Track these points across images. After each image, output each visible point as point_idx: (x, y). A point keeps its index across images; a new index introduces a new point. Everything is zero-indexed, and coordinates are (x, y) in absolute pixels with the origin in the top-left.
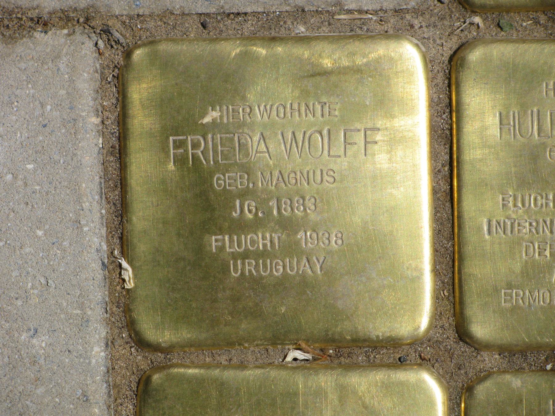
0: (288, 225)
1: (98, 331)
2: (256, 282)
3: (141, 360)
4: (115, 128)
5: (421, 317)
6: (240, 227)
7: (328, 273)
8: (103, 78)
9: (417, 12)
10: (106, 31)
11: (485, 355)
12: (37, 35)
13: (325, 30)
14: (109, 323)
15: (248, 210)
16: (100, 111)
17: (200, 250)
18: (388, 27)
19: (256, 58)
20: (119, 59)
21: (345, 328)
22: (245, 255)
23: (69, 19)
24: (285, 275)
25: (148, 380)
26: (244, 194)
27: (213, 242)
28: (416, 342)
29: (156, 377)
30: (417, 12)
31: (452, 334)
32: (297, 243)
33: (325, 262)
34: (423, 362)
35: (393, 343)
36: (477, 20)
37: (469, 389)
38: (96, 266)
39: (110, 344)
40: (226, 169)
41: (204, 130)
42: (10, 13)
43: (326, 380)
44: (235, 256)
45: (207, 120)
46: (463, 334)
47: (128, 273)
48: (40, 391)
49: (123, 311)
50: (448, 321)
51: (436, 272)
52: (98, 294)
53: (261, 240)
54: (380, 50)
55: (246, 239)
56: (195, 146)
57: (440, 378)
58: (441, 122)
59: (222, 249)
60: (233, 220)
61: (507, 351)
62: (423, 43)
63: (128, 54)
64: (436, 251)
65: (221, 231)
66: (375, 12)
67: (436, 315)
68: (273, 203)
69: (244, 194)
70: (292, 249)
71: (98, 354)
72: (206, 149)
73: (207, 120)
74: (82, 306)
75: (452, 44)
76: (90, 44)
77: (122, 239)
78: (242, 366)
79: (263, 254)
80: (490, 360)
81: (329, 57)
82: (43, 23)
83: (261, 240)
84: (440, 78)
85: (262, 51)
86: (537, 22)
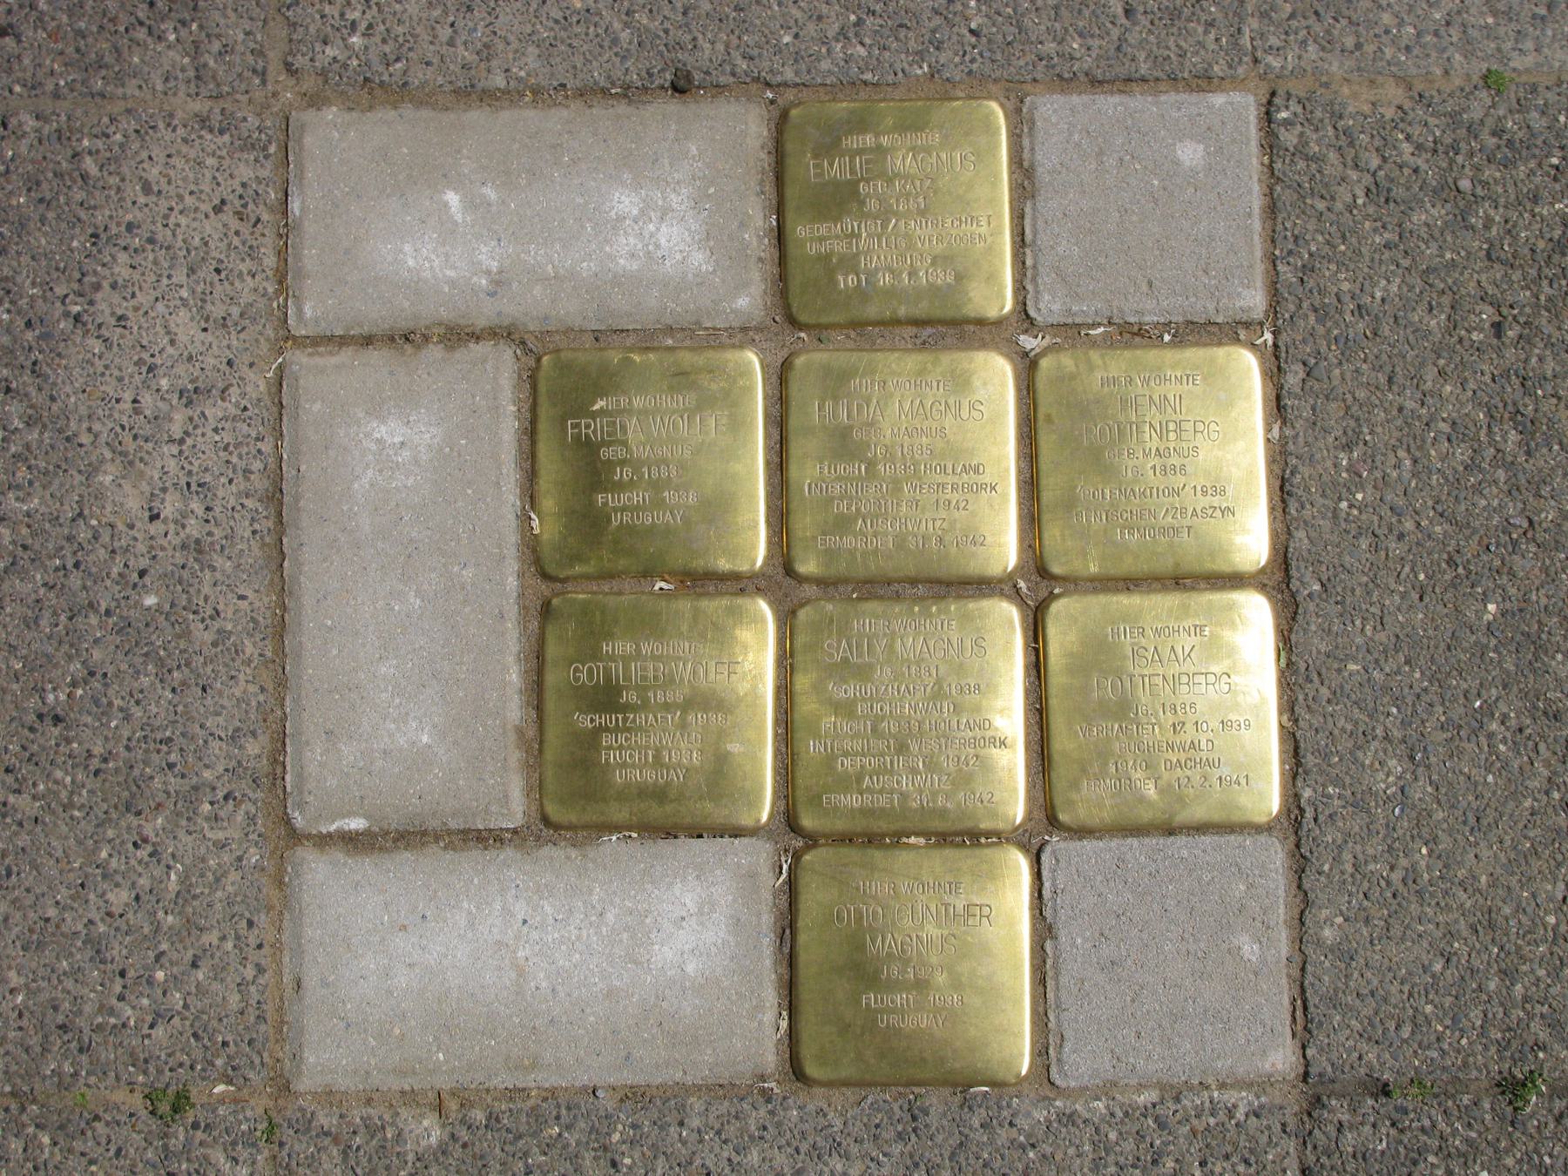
0: (657, 486)
1: (512, 566)
2: (630, 530)
3: (544, 588)
4: (528, 415)
5: (1018, 811)
6: (620, 487)
7: (687, 521)
8: (520, 376)
9: (758, 329)
10: (523, 343)
11: (806, 586)
12: (471, 345)
13: (688, 343)
14: (521, 560)
15: (625, 474)
16: (517, 401)
17: (591, 503)
18: (736, 341)
19: (633, 362)
20: (532, 363)
21: (699, 564)
22: (623, 509)
23: (495, 334)
24: (653, 525)
25: (549, 603)
26: (623, 463)
27: (600, 498)
28: (753, 576)
29: (555, 601)
30: (758, 329)
31: (781, 570)
32: (664, 499)
33: (1046, 893)
34: (759, 591)
35: (735, 577)
36: (803, 335)
37: (794, 612)
38: (512, 517)
39: (521, 575)
40: (609, 444)
41: (594, 415)
42: (452, 329)
43: (684, 605)
44: (615, 510)
45: (596, 407)
46: (789, 571)
47: (536, 523)
48: (467, 610)
49: (532, 550)
50: (778, 561)
51: (768, 522)
52: (512, 538)
53: (636, 497)
54: (732, 356)
55: (624, 497)
56: (588, 426)
57: (770, 603)
58: (775, 411)
59: (606, 504)
60: (614, 483)
61: (821, 582)
62: (761, 352)
63: (539, 360)
64: (768, 507)
65: (606, 491)
66: (726, 330)
67: (769, 557)
68: (645, 469)
69: (623, 463)
70: (659, 504)
71: (512, 582)
72: (594, 429)
73: (596, 407)
74: (499, 546)
75: (785, 353)
76: (509, 352)
77: (531, 496)
78: (620, 593)
79: (637, 508)
80: (810, 590)
81: (687, 358)
82: (476, 337)
83: (636, 497)
84: (774, 379)
85: (637, 358)
86: (848, 337)
